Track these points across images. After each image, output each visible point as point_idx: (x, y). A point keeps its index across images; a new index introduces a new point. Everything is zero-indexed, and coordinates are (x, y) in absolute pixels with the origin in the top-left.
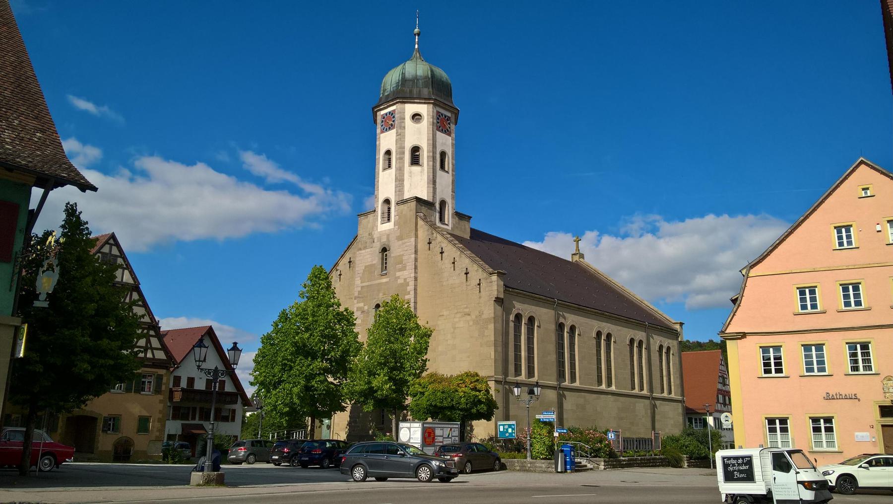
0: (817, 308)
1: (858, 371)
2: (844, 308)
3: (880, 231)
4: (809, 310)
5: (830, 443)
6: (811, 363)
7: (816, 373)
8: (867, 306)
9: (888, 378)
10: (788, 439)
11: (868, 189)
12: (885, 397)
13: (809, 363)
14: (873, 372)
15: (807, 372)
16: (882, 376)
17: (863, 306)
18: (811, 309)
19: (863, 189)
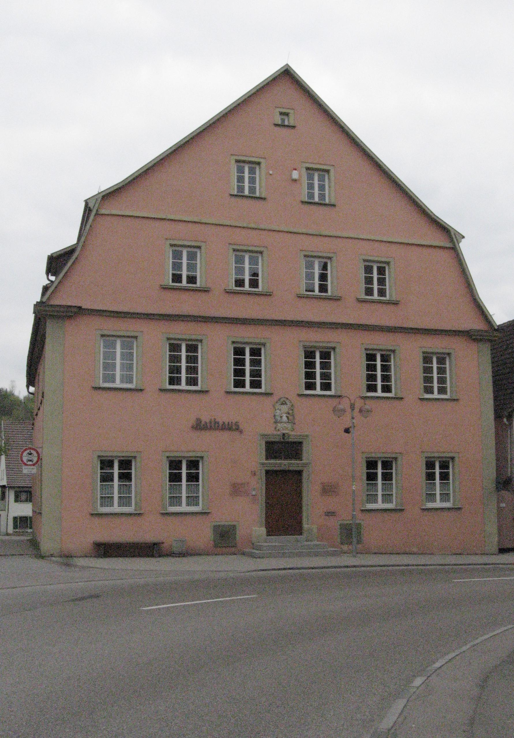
0: (195, 283)
1: (177, 384)
2: (171, 283)
3: (295, 181)
4: (376, 296)
5: (193, 500)
6: (178, 370)
7: (183, 386)
8: (204, 285)
9: (282, 400)
10: (449, 490)
11: (287, 114)
12: (276, 428)
13: (175, 370)
14: (262, 390)
15: (234, 387)
16: (275, 398)
17: (260, 289)
18: (188, 283)
19: (281, 114)
